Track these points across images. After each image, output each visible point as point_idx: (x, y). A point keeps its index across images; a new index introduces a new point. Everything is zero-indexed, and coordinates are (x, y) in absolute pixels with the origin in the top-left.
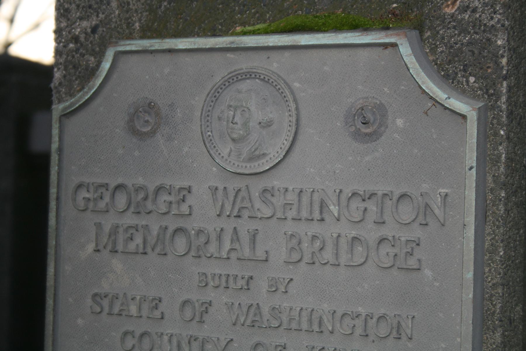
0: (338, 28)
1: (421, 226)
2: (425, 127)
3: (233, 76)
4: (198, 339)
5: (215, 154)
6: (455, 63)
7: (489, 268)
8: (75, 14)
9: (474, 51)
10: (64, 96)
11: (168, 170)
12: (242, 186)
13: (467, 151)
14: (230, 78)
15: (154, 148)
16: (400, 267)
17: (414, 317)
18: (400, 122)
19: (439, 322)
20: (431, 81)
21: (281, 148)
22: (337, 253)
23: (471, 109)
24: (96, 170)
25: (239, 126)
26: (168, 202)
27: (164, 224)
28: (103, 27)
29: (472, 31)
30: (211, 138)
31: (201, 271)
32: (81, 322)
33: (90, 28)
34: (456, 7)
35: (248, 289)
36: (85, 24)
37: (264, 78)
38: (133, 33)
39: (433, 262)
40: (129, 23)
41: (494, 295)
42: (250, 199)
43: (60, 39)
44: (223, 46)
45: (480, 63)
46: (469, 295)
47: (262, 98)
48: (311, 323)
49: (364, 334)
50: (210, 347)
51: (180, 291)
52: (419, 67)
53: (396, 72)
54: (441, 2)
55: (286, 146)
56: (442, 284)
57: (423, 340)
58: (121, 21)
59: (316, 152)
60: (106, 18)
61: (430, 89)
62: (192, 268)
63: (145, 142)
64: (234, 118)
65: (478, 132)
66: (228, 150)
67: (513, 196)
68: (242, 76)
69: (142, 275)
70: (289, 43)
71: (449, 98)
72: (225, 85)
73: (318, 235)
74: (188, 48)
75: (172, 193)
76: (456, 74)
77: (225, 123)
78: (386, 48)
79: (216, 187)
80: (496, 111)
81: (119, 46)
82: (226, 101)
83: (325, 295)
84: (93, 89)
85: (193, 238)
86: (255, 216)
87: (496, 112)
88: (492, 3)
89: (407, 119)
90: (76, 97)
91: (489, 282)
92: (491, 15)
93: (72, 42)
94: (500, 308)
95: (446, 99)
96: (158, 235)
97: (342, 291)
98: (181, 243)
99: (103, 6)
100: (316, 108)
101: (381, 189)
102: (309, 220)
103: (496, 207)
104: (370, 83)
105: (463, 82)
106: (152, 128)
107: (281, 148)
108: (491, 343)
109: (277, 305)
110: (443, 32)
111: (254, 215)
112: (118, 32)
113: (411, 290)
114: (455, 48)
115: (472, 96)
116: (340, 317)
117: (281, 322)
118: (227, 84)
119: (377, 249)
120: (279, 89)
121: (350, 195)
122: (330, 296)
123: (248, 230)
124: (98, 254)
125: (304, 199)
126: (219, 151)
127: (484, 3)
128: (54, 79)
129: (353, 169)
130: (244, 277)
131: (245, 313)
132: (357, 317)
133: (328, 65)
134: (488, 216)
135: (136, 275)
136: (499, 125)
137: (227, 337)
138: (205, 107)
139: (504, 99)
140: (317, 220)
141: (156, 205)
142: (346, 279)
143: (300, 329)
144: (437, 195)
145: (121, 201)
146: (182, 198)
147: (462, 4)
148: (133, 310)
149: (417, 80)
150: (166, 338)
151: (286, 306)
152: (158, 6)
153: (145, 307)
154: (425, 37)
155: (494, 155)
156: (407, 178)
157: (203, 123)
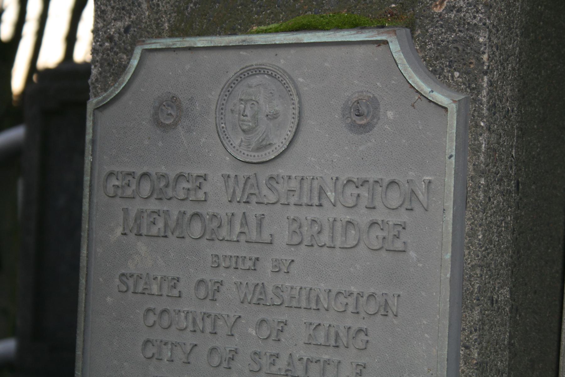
0: (339, 27)
1: (407, 211)
2: (412, 119)
3: (244, 72)
4: (211, 317)
5: (227, 144)
6: (442, 59)
7: (468, 251)
8: (110, 15)
9: (458, 48)
10: (99, 91)
11: (187, 159)
12: (251, 174)
13: (447, 141)
14: (241, 74)
15: (176, 139)
16: (388, 249)
17: (399, 296)
18: (390, 114)
19: (421, 300)
20: (417, 75)
21: (285, 139)
22: (333, 236)
23: (452, 101)
24: (125, 160)
25: (249, 118)
26: (186, 189)
27: (183, 210)
28: (134, 27)
29: (457, 29)
30: (224, 129)
31: (214, 253)
32: (109, 300)
33: (123, 28)
34: (443, 7)
35: (255, 270)
36: (119, 24)
37: (272, 73)
38: (163, 33)
39: (418, 244)
40: (158, 24)
41: (473, 276)
42: (257, 186)
43: (97, 39)
44: (236, 44)
45: (463, 59)
46: (447, 275)
47: (269, 92)
48: (309, 301)
49: (355, 311)
50: (221, 323)
51: (196, 272)
52: (406, 63)
53: (388, 67)
54: (431, 2)
55: (289, 137)
56: (425, 265)
57: (408, 317)
58: (150, 21)
59: (316, 142)
60: (137, 19)
61: (415, 84)
62: (206, 250)
63: (168, 134)
64: (244, 111)
65: (457, 123)
66: (240, 140)
67: (497, 184)
68: (252, 72)
69: (163, 257)
70: (293, 41)
71: (432, 91)
72: (237, 80)
73: (316, 219)
74: (205, 46)
75: (190, 181)
76: (443, 69)
77: (237, 115)
78: (379, 45)
79: (229, 175)
80: (477, 104)
81: (145, 44)
82: (239, 95)
83: (322, 275)
84: (123, 84)
85: (207, 222)
86: (261, 202)
87: (477, 105)
88: (475, 3)
89: (397, 111)
90: (108, 92)
91: (469, 264)
92: (474, 14)
93: (107, 42)
94: (477, 288)
95: (430, 92)
96: (178, 220)
97: (337, 271)
98: (197, 228)
99: (135, 7)
100: (317, 102)
101: (373, 176)
102: (309, 205)
103: (475, 194)
104: (365, 77)
105: (448, 77)
106: (174, 121)
107: (285, 139)
108: (469, 321)
109: (280, 285)
110: (432, 30)
111: (261, 201)
112: (148, 32)
113: (398, 271)
114: (442, 45)
115: (456, 90)
116: (335, 296)
117: (283, 300)
118: (239, 79)
119: (368, 232)
120: (284, 84)
121: (345, 182)
122: (326, 276)
123: (256, 215)
124: (125, 237)
125: (305, 186)
126: (232, 142)
127: (468, 3)
128: (91, 76)
129: (348, 158)
130: (252, 259)
131: (252, 292)
132: (349, 296)
133: (328, 62)
134: (469, 202)
135: (158, 257)
136: (480, 117)
137: (236, 314)
138: (219, 101)
139: (484, 93)
140: (316, 206)
141: (176, 192)
142: (341, 261)
143: (299, 306)
144: (422, 182)
145: (146, 188)
146: (198, 185)
147: (448, 4)
148: (155, 289)
149: (404, 75)
150: (183, 314)
151: (288, 286)
152: (185, 8)
153: (165, 286)
154: (415, 35)
155: (475, 145)
156: (396, 166)
157: (218, 115)
